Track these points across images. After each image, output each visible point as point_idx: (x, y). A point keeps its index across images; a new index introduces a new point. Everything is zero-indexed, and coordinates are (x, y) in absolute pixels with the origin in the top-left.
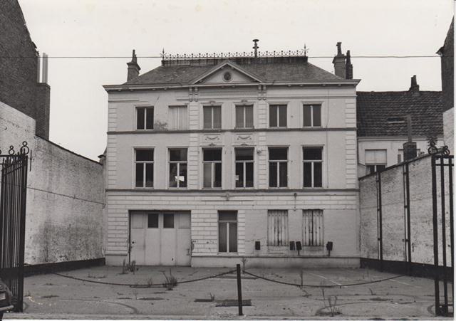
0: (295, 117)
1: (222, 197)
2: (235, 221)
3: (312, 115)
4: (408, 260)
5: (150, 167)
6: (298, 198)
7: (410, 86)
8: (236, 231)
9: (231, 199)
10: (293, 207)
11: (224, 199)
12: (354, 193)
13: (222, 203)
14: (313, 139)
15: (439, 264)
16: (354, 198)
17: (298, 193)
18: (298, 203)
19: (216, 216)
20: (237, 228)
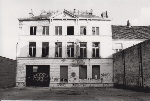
0: (89, 31)
1: (62, 60)
2: (33, 28)
3: (96, 31)
4: (142, 85)
5: (35, 49)
6: (90, 61)
7: (127, 24)
8: (79, 76)
9: (65, 61)
10: (88, 64)
11: (63, 61)
12: (111, 59)
13: (62, 63)
14: (96, 39)
15: (37, 68)
16: (111, 61)
17: (91, 59)
18: (90, 63)
19: (59, 67)
20: (79, 77)
